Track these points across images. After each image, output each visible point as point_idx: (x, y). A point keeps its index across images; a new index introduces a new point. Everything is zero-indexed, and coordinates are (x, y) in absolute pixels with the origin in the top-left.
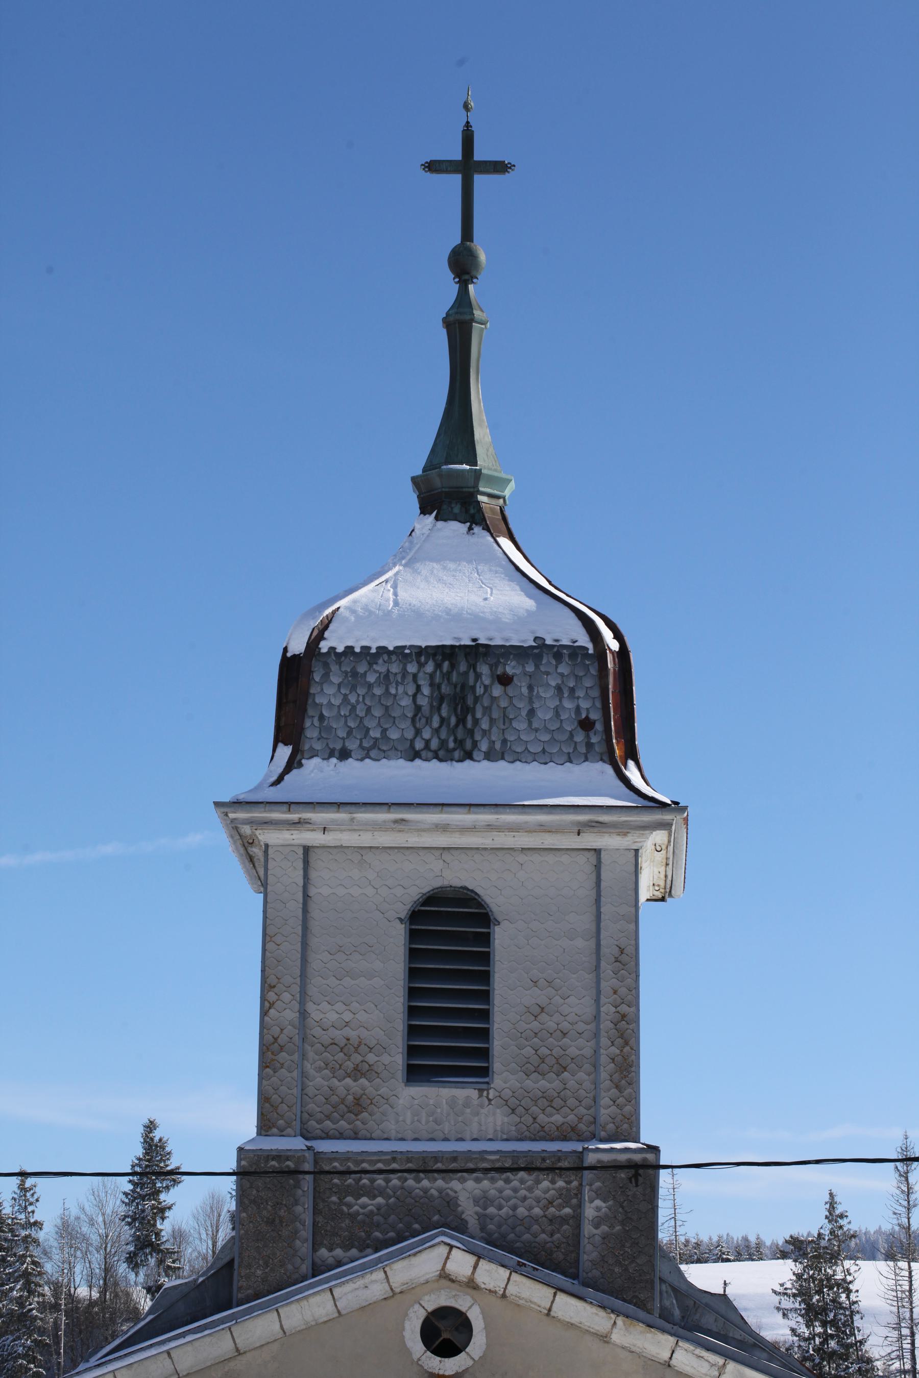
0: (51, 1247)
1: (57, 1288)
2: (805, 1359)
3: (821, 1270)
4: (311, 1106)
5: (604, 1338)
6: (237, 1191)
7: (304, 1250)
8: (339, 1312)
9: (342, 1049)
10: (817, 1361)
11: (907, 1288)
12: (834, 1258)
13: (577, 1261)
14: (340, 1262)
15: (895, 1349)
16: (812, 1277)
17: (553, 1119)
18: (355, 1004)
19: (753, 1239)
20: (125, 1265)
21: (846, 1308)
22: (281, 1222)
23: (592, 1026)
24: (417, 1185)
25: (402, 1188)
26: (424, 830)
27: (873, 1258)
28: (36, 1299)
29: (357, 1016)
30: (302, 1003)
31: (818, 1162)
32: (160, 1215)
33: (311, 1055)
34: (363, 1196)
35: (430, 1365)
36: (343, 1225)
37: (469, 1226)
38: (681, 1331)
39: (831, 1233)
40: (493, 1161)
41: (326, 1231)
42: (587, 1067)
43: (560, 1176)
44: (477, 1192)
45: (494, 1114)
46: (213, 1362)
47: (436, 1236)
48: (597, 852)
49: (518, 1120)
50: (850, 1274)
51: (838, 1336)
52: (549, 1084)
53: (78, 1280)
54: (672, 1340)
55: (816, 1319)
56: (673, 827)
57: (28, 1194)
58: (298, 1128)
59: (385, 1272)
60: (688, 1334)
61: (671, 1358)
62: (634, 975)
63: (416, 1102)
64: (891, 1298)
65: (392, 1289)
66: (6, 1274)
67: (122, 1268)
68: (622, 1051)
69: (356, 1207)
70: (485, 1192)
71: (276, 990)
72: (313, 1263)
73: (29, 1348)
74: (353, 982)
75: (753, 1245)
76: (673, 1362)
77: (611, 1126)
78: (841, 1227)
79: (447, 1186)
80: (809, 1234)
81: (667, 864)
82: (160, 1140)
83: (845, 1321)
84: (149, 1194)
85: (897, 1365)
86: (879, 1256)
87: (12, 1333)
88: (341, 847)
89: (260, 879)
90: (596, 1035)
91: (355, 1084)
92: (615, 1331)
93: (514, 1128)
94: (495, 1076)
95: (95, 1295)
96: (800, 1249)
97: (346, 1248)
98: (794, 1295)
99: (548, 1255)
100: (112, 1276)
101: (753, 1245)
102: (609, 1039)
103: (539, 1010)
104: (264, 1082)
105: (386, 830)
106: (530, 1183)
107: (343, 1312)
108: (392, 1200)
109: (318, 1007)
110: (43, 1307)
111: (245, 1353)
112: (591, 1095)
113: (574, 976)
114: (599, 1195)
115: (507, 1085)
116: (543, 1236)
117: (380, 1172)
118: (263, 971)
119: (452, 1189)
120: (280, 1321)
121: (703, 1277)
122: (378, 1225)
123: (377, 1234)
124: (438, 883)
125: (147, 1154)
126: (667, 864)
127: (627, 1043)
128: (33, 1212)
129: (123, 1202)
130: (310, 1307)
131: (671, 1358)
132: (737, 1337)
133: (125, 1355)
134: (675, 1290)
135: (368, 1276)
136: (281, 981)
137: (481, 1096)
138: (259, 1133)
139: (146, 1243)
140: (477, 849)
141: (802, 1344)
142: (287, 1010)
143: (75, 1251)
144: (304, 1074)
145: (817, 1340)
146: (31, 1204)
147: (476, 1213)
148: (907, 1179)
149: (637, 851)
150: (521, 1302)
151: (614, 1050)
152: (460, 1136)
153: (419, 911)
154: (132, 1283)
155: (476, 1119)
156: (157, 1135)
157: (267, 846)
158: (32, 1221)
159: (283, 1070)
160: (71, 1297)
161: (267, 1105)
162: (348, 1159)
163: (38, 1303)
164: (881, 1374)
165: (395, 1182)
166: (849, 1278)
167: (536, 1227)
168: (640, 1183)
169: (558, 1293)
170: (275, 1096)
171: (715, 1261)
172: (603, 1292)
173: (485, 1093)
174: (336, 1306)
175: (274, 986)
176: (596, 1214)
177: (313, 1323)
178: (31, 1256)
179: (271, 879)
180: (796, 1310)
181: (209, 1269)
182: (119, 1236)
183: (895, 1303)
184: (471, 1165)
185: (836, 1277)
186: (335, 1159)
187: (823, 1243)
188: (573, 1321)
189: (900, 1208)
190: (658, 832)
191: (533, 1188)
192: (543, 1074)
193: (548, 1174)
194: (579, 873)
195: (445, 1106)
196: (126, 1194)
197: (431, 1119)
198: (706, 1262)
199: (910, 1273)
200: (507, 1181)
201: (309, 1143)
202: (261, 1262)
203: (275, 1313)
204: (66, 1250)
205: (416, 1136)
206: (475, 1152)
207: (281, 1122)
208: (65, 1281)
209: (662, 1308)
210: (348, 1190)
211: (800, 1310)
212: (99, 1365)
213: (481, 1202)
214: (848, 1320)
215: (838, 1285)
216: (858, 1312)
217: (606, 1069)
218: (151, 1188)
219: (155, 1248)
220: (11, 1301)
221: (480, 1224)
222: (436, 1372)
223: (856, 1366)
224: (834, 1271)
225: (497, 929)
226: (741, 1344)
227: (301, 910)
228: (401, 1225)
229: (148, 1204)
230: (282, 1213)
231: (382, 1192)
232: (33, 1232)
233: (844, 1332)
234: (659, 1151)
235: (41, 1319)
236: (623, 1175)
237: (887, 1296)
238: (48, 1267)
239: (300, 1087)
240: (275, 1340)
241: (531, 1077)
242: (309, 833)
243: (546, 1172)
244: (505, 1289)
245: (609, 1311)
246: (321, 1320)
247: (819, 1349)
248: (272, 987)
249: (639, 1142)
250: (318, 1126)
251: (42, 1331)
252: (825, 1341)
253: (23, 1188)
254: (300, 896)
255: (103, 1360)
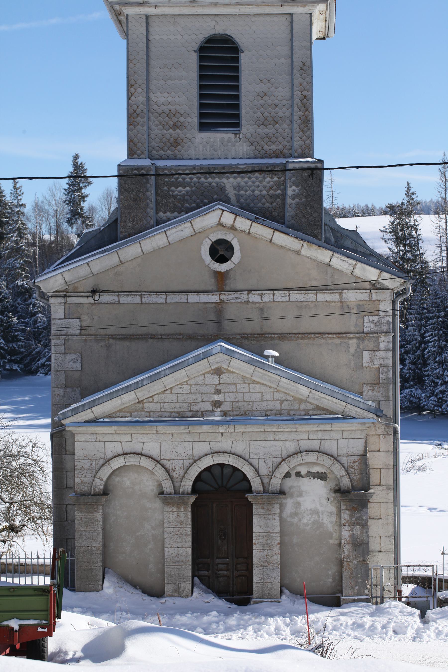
0: (30, 216)
1: (34, 235)
2: (395, 262)
3: (403, 220)
4: (153, 144)
5: (298, 253)
6: (118, 187)
7: (151, 213)
8: (169, 242)
9: (167, 115)
10: (401, 262)
11: (445, 227)
12: (409, 214)
13: (284, 216)
14: (169, 218)
15: (438, 256)
16: (399, 223)
17: (271, 148)
18: (173, 93)
19: (370, 206)
20: (66, 224)
21: (415, 238)
22: (140, 200)
23: (290, 102)
24: (206, 181)
25: (199, 182)
26: (205, 6)
27: (428, 214)
28: (24, 241)
29: (174, 99)
30: (147, 93)
31: (400, 165)
32: (83, 199)
33: (152, 118)
34: (180, 186)
35: (214, 267)
36: (170, 201)
37: (231, 200)
38: (335, 249)
39: (408, 202)
40: (242, 168)
41: (162, 204)
42: (288, 122)
43: (275, 175)
44: (235, 184)
45: (243, 146)
46: (109, 267)
47: (215, 205)
48: (291, 15)
49: (254, 148)
50: (417, 221)
51: (411, 251)
52: (269, 130)
53: (44, 231)
54: (331, 253)
55: (401, 243)
56: (329, 2)
57: (18, 191)
58: (147, 154)
59: (191, 223)
60: (338, 250)
61: (330, 261)
62: (310, 76)
63: (204, 140)
64: (437, 232)
65: (195, 231)
66: (9, 229)
67: (65, 225)
68: (304, 113)
69: (176, 192)
70: (239, 184)
71: (134, 87)
72: (156, 220)
73: (22, 264)
74: (172, 82)
75: (370, 208)
76: (331, 263)
77: (300, 151)
78: (413, 199)
79: (220, 181)
80: (397, 203)
81: (326, 21)
82: (81, 163)
83: (415, 244)
84: (77, 190)
85: (439, 264)
86: (431, 212)
87: (13, 257)
88: (165, 15)
89: (125, 32)
90: (292, 106)
91: (174, 132)
92: (303, 249)
93: (252, 152)
94: (243, 127)
95: (53, 238)
96: (393, 210)
97: (172, 212)
98: (390, 232)
99: (270, 214)
100: (60, 229)
101: (370, 208)
102: (298, 108)
103: (263, 94)
104: (130, 132)
105: (187, 6)
106: (261, 179)
107: (171, 243)
108: (194, 188)
109: (155, 95)
110: (27, 244)
111: (125, 263)
112: (290, 135)
113: (281, 77)
114: (294, 184)
115: (249, 131)
116: (268, 204)
117: (187, 174)
118: (128, 78)
119: (223, 183)
120: (141, 248)
121: (346, 223)
122: (187, 201)
123: (187, 205)
124: (212, 32)
125: (75, 170)
126: (326, 21)
127: (307, 110)
128: (21, 199)
129: (64, 194)
130: (155, 241)
131: (330, 261)
132: (362, 251)
133: (67, 265)
134: (332, 229)
135: (183, 225)
136: (137, 82)
137: (236, 137)
138: (128, 157)
139: (76, 213)
140: (232, 15)
141: (394, 255)
142: (140, 97)
143: (42, 218)
144: (149, 128)
145: (401, 253)
146: (20, 195)
147: (235, 194)
148: (445, 176)
149: (311, 14)
150: (257, 236)
151: (301, 113)
152: (226, 157)
153: (204, 46)
154: (70, 232)
155: (234, 148)
156: (79, 161)
157: (128, 15)
158: (21, 203)
159: (139, 126)
160: (41, 240)
161: (132, 143)
162: (172, 169)
163: (25, 243)
164: (432, 268)
165: (195, 179)
166: (417, 223)
167: (264, 200)
168: (314, 178)
169: (275, 231)
170: (135, 139)
171: (352, 216)
172: (297, 230)
173: (238, 136)
174: (168, 240)
175: (133, 85)
176: (293, 193)
177: (157, 248)
178: (21, 220)
179: (130, 32)
180: (391, 239)
181: (105, 224)
182: (63, 210)
183: (439, 235)
184: (231, 171)
185: (410, 223)
186: (165, 169)
187: (404, 207)
188: (282, 245)
189: (442, 189)
190: (321, 4)
191: (262, 181)
192: (266, 126)
193: (269, 174)
194: (282, 25)
195: (219, 143)
196: (65, 190)
197: (212, 149)
198: (348, 217)
199: (446, 220)
200: (250, 178)
201: (153, 162)
202: (131, 219)
203: (139, 244)
204: (38, 217)
205: (205, 157)
206: (233, 165)
207: (139, 152)
208: (38, 232)
209: (326, 238)
210: (172, 184)
211: (393, 239)
212: (54, 270)
213: (237, 188)
214: (416, 244)
215: (412, 227)
216: (421, 239)
217: (297, 123)
218: (78, 187)
219: (81, 216)
220: (12, 242)
221: (237, 199)
222: (217, 270)
223: (420, 265)
224: (410, 220)
225: (242, 54)
226: (364, 254)
227: (145, 47)
228: (198, 200)
229: (76, 194)
230: (140, 196)
231: (188, 185)
232: (21, 209)
233: (414, 249)
234: (323, 162)
235: (27, 250)
236: (306, 174)
237: (435, 232)
238: (29, 226)
239: (147, 134)
240: (139, 257)
241: (261, 127)
242: (149, 8)
243: (268, 173)
244: (249, 230)
245: (300, 239)
246: (161, 247)
247: (402, 257)
248: (132, 85)
249: (313, 158)
250: (157, 153)
251: (28, 256)
252: (405, 254)
253: (15, 188)
254: (145, 40)
255: (56, 268)
